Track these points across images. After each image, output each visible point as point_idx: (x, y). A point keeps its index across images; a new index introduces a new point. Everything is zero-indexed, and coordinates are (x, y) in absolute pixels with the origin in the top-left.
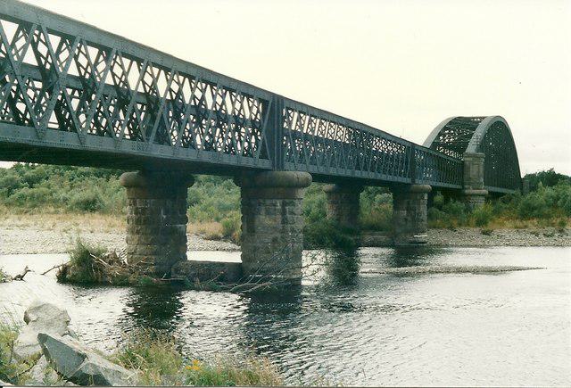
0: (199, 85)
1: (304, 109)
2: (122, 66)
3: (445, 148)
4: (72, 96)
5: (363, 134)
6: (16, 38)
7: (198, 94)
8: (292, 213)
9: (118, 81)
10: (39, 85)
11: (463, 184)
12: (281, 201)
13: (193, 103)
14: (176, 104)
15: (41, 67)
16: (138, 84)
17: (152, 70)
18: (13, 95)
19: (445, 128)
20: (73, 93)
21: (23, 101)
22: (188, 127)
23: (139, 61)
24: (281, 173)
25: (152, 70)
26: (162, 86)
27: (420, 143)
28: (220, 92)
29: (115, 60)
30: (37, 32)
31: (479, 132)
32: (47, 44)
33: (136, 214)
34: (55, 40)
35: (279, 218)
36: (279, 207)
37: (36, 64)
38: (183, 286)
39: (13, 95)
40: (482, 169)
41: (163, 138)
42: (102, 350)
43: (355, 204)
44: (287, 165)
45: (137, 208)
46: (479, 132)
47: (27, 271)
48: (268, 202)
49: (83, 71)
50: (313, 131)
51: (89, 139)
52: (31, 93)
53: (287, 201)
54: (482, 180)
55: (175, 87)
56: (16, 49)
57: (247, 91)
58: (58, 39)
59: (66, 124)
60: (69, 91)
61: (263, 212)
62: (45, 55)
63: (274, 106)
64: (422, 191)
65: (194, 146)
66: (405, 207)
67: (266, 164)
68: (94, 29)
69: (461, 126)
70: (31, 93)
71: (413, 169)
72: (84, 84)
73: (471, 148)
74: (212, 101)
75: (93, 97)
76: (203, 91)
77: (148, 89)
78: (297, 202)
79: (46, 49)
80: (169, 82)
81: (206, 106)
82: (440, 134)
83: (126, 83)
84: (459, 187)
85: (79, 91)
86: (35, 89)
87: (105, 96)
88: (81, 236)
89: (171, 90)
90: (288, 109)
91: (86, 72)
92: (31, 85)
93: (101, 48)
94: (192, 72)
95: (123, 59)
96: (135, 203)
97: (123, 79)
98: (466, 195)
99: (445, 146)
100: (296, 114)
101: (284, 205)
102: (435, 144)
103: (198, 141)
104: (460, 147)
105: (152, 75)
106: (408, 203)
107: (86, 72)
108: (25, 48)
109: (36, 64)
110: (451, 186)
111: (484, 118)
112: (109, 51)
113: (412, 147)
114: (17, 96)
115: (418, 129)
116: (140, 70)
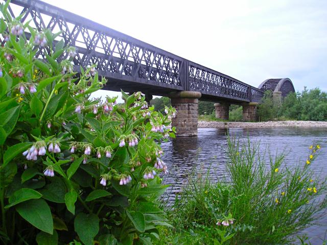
1: (199, 67)
2: (148, 54)
5: (229, 80)
6: (94, 37)
16: (142, 56)
27: (257, 87)
31: (280, 83)
32: (106, 39)
34: (92, 33)
35: (187, 111)
36: (187, 107)
43: (4, 175)
46: (280, 83)
47: (305, 87)
48: (182, 105)
53: (190, 104)
57: (172, 57)
62: (65, 31)
63: (184, 64)
66: (247, 111)
68: (170, 53)
69: (272, 83)
76: (169, 62)
79: (39, 20)
80: (164, 60)
91: (122, 51)
93: (54, 16)
100: (206, 73)
101: (189, 105)
107: (122, 51)
108: (97, 41)
111: (281, 79)
112: (80, 25)
115: (256, 82)
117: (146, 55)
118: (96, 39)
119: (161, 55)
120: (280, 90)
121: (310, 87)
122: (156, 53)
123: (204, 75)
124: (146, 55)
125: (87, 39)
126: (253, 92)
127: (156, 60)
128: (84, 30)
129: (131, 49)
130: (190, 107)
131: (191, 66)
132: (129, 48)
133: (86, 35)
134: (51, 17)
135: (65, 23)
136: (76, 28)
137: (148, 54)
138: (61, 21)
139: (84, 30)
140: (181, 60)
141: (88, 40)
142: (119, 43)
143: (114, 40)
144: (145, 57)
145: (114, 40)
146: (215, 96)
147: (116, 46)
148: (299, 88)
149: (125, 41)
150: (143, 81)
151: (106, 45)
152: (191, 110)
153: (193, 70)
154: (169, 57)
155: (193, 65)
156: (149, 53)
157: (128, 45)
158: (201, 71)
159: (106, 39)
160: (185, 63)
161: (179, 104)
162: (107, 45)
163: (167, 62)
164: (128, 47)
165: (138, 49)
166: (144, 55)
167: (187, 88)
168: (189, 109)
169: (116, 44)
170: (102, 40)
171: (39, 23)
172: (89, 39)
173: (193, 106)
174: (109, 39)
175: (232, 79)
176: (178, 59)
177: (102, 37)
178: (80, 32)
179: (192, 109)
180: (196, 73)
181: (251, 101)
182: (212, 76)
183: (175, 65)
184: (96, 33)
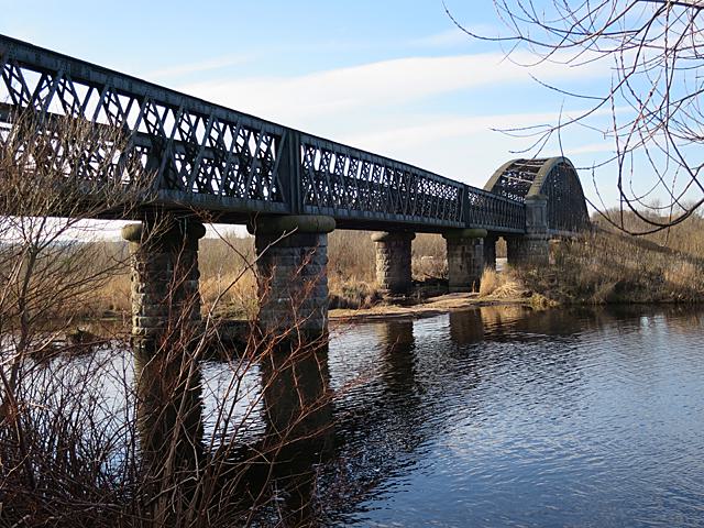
0: (264, 138)
1: (327, 146)
5: (412, 175)
6: (39, 88)
9: (152, 129)
14: (190, 148)
16: (138, 122)
20: (142, 150)
22: (254, 179)
25: (244, 133)
26: (228, 139)
28: (264, 138)
29: (148, 107)
30: (9, 66)
32: (73, 92)
38: (479, 339)
41: (564, 239)
46: (542, 175)
50: (377, 179)
55: (264, 147)
56: (39, 99)
57: (254, 125)
60: (139, 149)
63: (289, 139)
64: (476, 237)
65: (262, 198)
67: (281, 207)
71: (466, 213)
72: (153, 141)
73: (533, 192)
74: (255, 146)
76: (247, 139)
77: (214, 143)
81: (249, 153)
82: (501, 178)
83: (161, 131)
85: (148, 149)
88: (637, 289)
89: (237, 145)
90: (308, 147)
91: (155, 129)
94: (256, 125)
97: (158, 127)
99: (510, 189)
102: (497, 188)
103: (266, 193)
104: (522, 190)
108: (49, 98)
110: (512, 230)
113: (464, 190)
115: (479, 177)
116: (206, 126)
117: (185, 127)
118: (44, 93)
119: (226, 123)
120: (543, 190)
123: (343, 168)
124: (215, 134)
125: (21, 96)
126: (473, 199)
127: (211, 138)
129: (194, 134)
131: (308, 147)
132: (98, 98)
134: (40, 75)
135: (149, 129)
136: (45, 83)
138: (9, 66)
140: (278, 132)
141: (22, 99)
142: (110, 99)
143: (95, 91)
144: (181, 131)
145: (95, 91)
148: (600, 197)
149: (161, 104)
151: (73, 108)
153: (313, 157)
154: (269, 134)
155: (314, 142)
156: (221, 125)
157: (135, 101)
159: (73, 92)
162: (76, 108)
163: (240, 141)
164: (136, 109)
165: (161, 110)
166: (178, 125)
169: (102, 102)
170: (61, 95)
172: (25, 96)
174: (81, 90)
177: (61, 88)
178: (32, 92)
180: (322, 163)
182: (375, 170)
183: (264, 147)
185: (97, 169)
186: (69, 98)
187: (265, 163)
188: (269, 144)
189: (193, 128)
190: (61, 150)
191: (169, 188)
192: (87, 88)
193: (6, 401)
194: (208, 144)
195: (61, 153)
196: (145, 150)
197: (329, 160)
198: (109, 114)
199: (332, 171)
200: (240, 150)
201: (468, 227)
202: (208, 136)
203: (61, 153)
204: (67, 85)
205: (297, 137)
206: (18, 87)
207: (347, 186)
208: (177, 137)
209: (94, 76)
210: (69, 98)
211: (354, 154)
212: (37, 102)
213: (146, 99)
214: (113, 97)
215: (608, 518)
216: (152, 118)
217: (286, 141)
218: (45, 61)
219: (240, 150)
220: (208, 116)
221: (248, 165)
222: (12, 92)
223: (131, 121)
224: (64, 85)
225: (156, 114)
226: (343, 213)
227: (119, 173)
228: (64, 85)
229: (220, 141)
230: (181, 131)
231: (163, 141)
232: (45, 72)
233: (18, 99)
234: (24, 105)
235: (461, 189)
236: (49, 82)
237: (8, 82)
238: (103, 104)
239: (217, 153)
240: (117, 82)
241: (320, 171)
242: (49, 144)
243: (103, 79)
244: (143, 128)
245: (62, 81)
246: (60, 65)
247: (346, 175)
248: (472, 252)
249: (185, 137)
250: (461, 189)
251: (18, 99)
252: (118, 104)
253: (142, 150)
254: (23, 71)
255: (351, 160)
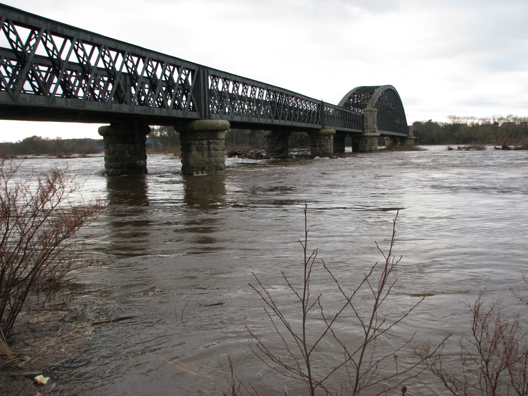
1: (227, 77)
3: (354, 106)
4: (71, 75)
6: (29, 39)
7: (183, 77)
8: (215, 149)
9: (130, 70)
10: (106, 79)
11: (363, 130)
12: (207, 141)
13: (180, 82)
14: (132, 77)
15: (14, 50)
17: (169, 68)
18: (92, 86)
19: (354, 94)
20: (72, 73)
21: (98, 89)
23: (178, 67)
24: (208, 121)
25: (169, 68)
27: (336, 103)
30: (45, 34)
33: (109, 154)
35: (206, 154)
37: (77, 62)
39: (92, 86)
40: (375, 119)
42: (346, 190)
44: (326, 127)
45: (110, 151)
48: (197, 142)
49: (107, 65)
51: (156, 109)
52: (102, 84)
53: (211, 141)
54: (376, 127)
55: (183, 77)
57: (178, 64)
58: (115, 53)
59: (68, 92)
60: (69, 72)
61: (195, 149)
63: (200, 72)
64: (329, 135)
67: (195, 115)
69: (362, 95)
70: (102, 84)
75: (137, 84)
76: (187, 76)
77: (168, 78)
78: (219, 141)
80: (180, 73)
82: (350, 98)
83: (135, 72)
84: (361, 131)
86: (103, 81)
87: (142, 83)
89: (181, 79)
91: (110, 66)
92: (8, 63)
95: (133, 57)
96: (108, 147)
97: (134, 69)
98: (365, 137)
101: (209, 144)
105: (170, 71)
106: (320, 142)
107: (110, 66)
109: (77, 62)
113: (321, 104)
114: (94, 86)
115: (333, 95)
116: (179, 72)
118: (32, 43)
121: (423, 119)
122: (146, 60)
123: (255, 94)
124: (168, 73)
128: (46, 37)
130: (211, 146)
131: (214, 77)
133: (50, 46)
136: (33, 36)
137: (152, 66)
138: (7, 24)
139: (46, 37)
140: (193, 67)
142: (105, 53)
144: (148, 71)
145: (120, 55)
146: (258, 124)
147: (73, 51)
149: (135, 55)
150: (164, 113)
152: (213, 152)
154: (187, 69)
155: (217, 74)
157: (141, 60)
158: (250, 88)
160: (201, 72)
161: (192, 142)
162: (85, 59)
164: (120, 58)
165: (135, 59)
167: (205, 114)
168: (209, 149)
169: (73, 47)
171: (15, 40)
172: (55, 52)
173: (216, 144)
174: (88, 48)
175: (289, 93)
176: (188, 66)
178: (41, 42)
179: (215, 149)
180: (243, 91)
181: (323, 128)
184: (32, 33)
185: (98, 94)
186: (81, 53)
187: (184, 86)
188: (187, 76)
189: (155, 70)
190: (78, 82)
191: (176, 109)
192: (91, 47)
193: (3, 242)
194: (164, 79)
195: (77, 84)
196: (74, 74)
197: (238, 88)
198: (105, 62)
199: (257, 98)
200: (183, 82)
201: (364, 132)
202: (163, 74)
203: (77, 84)
204: (80, 45)
205: (206, 70)
206: (13, 37)
207: (257, 104)
208: (145, 75)
209: (67, 32)
210: (81, 53)
211: (246, 82)
212: (28, 48)
213: (103, 46)
214: (106, 52)
215: (438, 361)
216: (130, 64)
217: (199, 73)
218: (31, 22)
219: (183, 82)
220: (180, 67)
221: (172, 88)
222: (11, 41)
223: (139, 71)
224: (78, 45)
225: (132, 62)
226: (237, 119)
227: (77, 91)
228: (78, 45)
229: (171, 77)
230: (148, 71)
231: (115, 73)
232: (33, 29)
233: (51, 53)
234: (55, 57)
235: (319, 105)
236: (36, 35)
237: (7, 34)
238: (101, 56)
239: (84, 69)
240: (82, 36)
241: (242, 95)
242: (69, 80)
243: (72, 33)
244: (125, 70)
245: (77, 43)
246: (42, 25)
247: (249, 96)
248: (325, 144)
249: (150, 74)
250: (319, 105)
251: (51, 53)
252: (109, 56)
253: (72, 73)
254: (53, 37)
255: (260, 89)
